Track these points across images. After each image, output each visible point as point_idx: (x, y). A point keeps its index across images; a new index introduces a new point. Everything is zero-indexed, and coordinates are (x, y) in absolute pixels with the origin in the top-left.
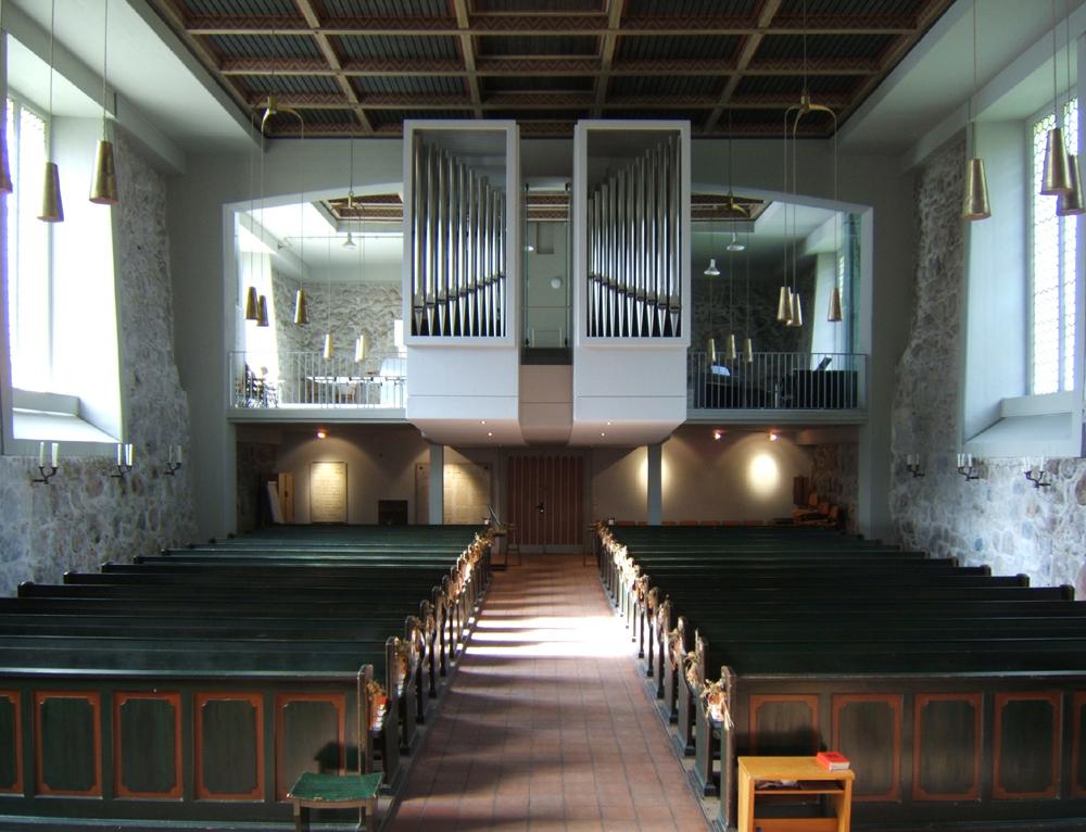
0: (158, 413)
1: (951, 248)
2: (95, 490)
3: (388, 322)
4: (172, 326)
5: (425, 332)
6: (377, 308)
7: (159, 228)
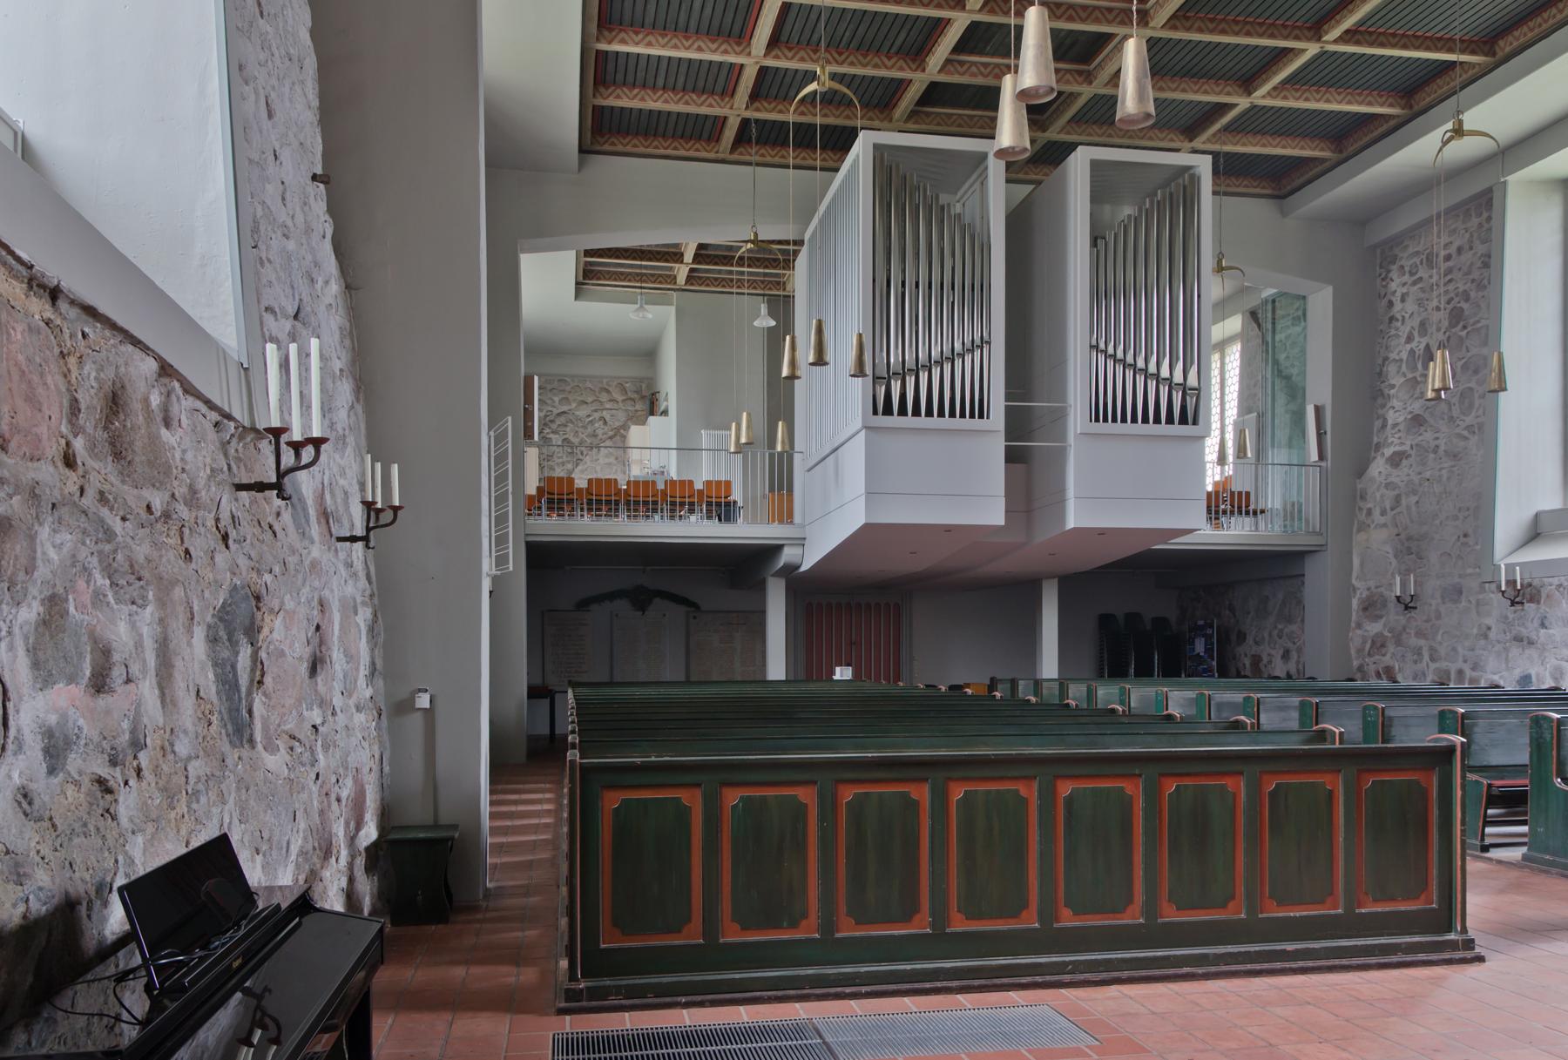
1: (1464, 333)
5: (888, 411)
6: (582, 412)
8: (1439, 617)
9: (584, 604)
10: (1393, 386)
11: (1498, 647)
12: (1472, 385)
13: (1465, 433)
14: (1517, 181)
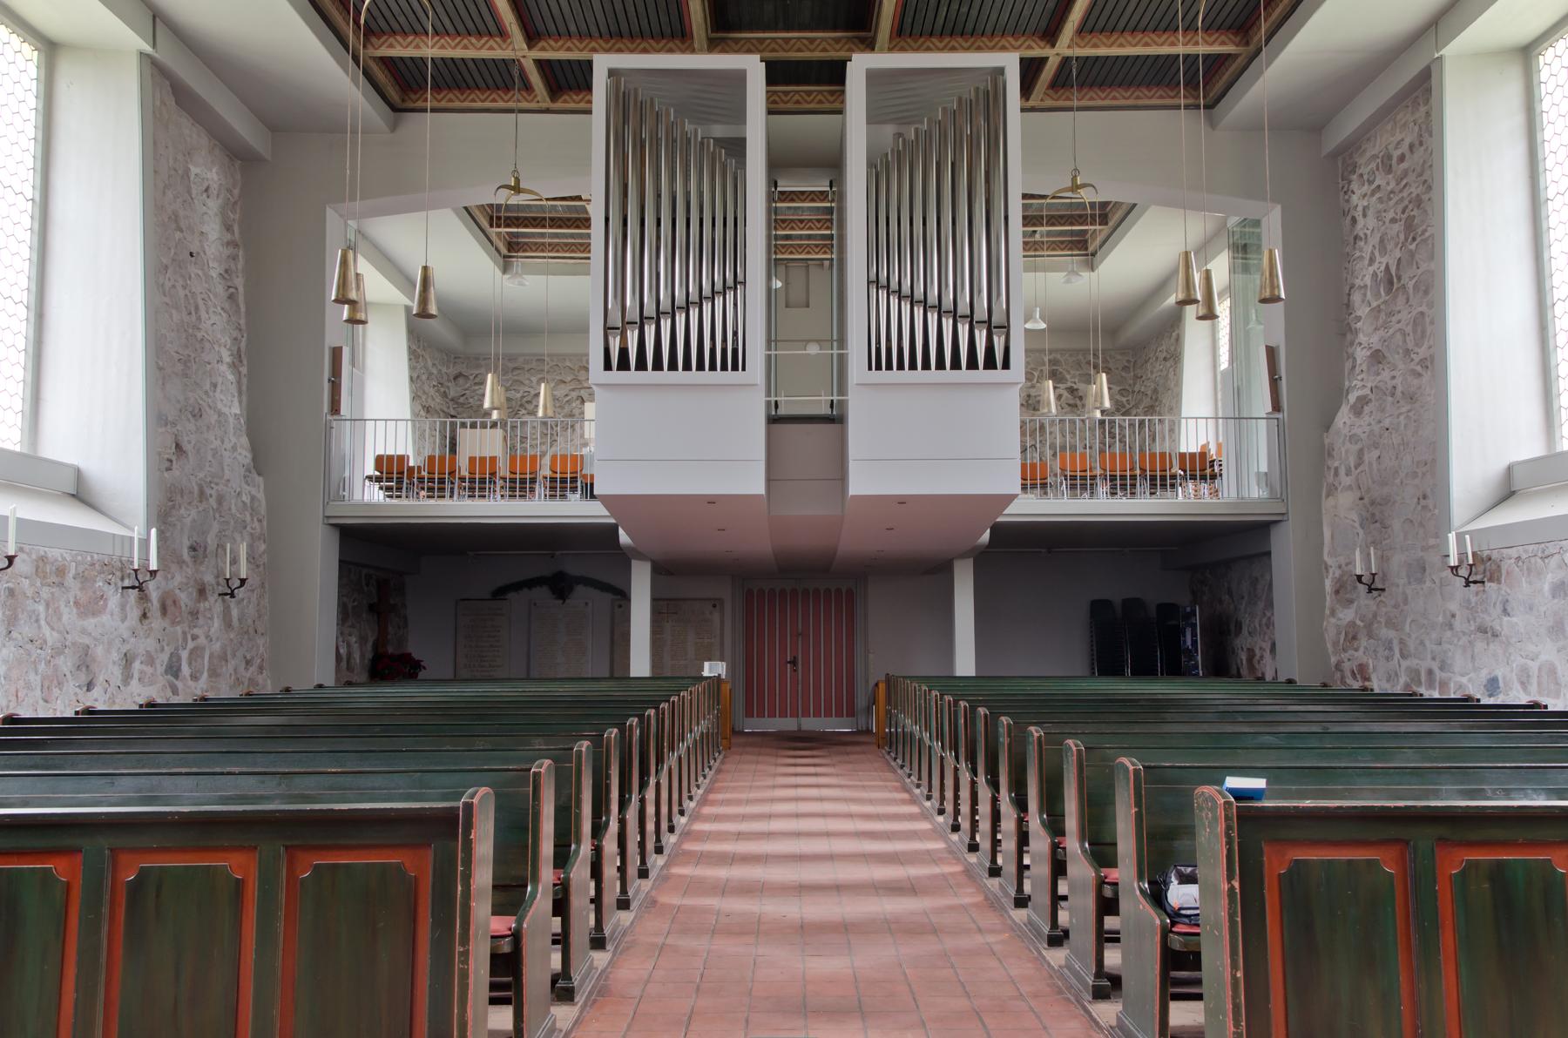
0: (213, 502)
1: (1413, 247)
2: (91, 607)
3: (576, 412)
4: (245, 381)
5: (624, 365)
7: (229, 237)
8: (1406, 601)
9: (500, 593)
10: (1359, 319)
11: (1464, 639)
12: (1423, 308)
13: (1419, 368)
14: (1456, 49)
